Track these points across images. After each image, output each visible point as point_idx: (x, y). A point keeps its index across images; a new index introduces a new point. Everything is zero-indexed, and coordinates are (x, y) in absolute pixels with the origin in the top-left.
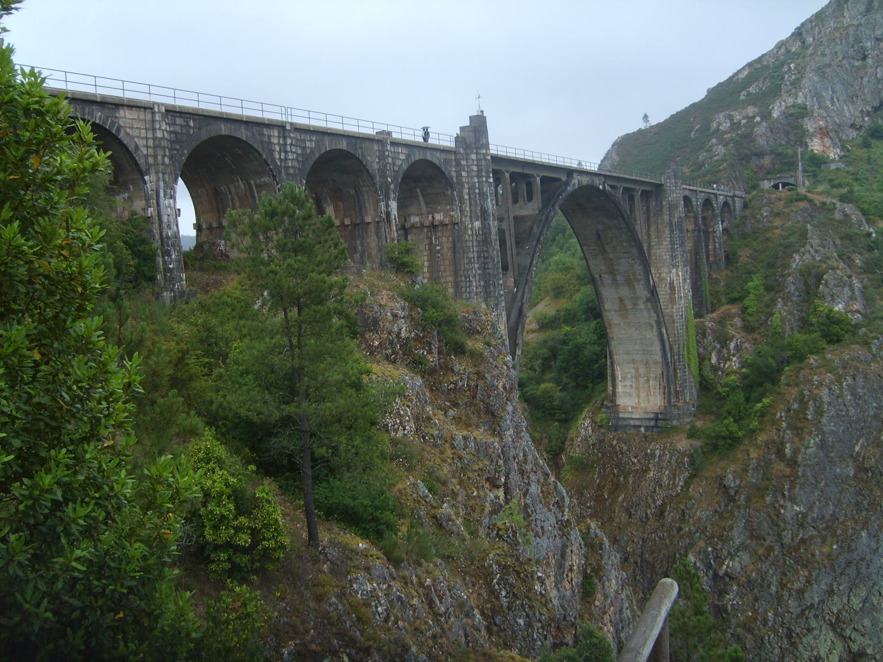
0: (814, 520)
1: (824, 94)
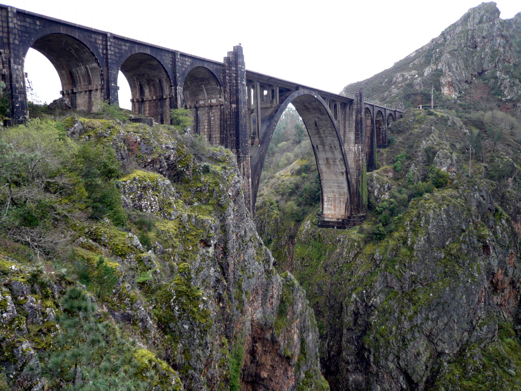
0: (421, 279)
1: (453, 65)
